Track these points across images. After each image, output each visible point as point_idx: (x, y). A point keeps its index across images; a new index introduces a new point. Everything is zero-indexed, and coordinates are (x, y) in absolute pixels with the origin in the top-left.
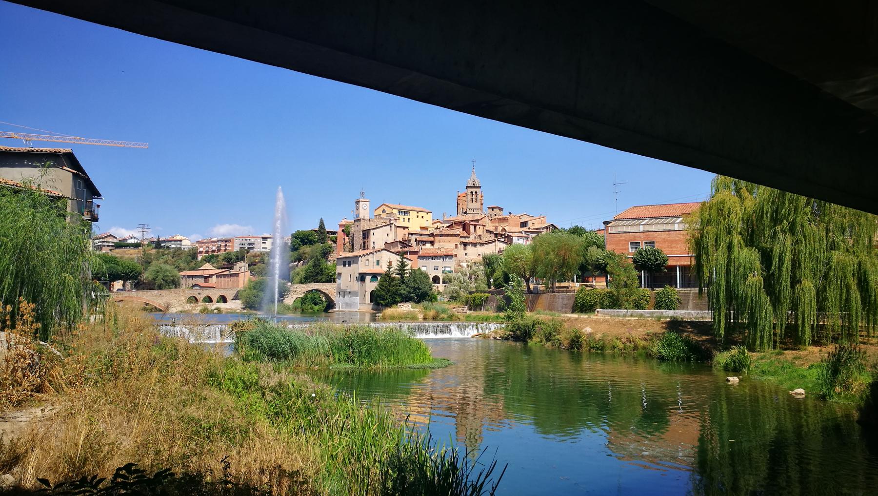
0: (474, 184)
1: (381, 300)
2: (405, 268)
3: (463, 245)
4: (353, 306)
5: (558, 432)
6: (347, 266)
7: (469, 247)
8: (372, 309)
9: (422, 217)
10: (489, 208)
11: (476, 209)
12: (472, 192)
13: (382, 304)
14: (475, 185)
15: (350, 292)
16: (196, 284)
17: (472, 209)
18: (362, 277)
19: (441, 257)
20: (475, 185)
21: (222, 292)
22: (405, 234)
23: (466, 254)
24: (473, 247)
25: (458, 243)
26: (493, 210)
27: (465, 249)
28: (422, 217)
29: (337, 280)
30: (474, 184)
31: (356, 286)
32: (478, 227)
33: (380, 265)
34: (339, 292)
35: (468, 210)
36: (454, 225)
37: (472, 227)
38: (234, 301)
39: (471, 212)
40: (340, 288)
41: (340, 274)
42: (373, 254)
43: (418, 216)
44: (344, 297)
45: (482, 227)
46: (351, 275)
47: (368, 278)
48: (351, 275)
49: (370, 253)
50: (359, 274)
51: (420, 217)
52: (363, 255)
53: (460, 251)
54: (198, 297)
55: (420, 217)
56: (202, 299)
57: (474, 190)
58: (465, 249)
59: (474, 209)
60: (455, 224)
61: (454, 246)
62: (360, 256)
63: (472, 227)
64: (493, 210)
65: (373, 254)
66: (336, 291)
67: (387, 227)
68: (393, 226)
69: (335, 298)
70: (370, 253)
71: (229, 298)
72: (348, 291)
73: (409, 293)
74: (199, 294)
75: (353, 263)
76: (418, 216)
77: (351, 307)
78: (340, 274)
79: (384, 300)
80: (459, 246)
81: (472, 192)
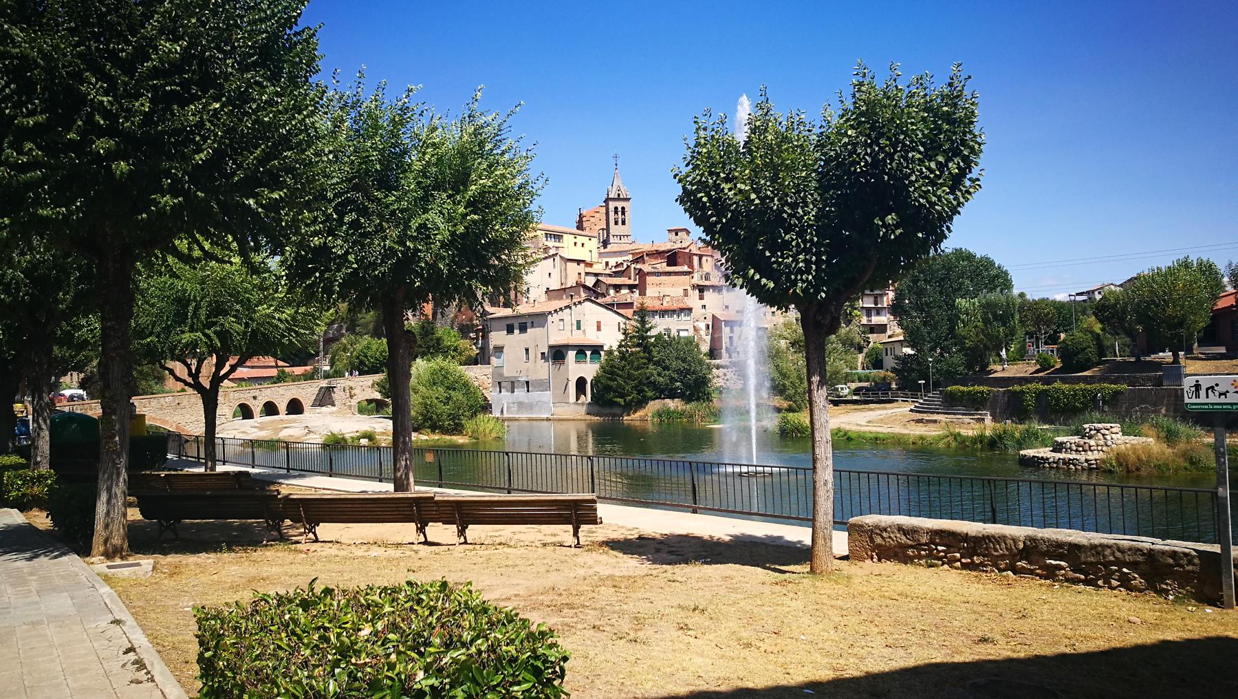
0: (619, 195)
1: (617, 397)
2: (649, 334)
3: (697, 291)
4: (536, 409)
5: (52, 552)
6: (517, 331)
7: (708, 294)
8: (588, 414)
9: (583, 245)
10: (670, 231)
11: (624, 236)
12: (616, 208)
13: (618, 404)
14: (621, 197)
15: (527, 383)
16: (177, 380)
17: (617, 236)
18: (557, 354)
19: (674, 311)
20: (621, 197)
21: (294, 392)
22: (580, 274)
23: (704, 307)
24: (716, 294)
25: (689, 288)
26: (677, 234)
27: (701, 298)
28: (583, 245)
29: (494, 360)
30: (619, 195)
31: (542, 370)
32: (704, 259)
33: (582, 328)
34: (499, 383)
35: (611, 237)
36: (646, 258)
37: (696, 259)
38: (319, 409)
39: (617, 240)
40: (501, 375)
41: (499, 350)
42: (570, 308)
43: (575, 243)
44: (513, 392)
45: (709, 259)
46: (527, 350)
47: (571, 354)
48: (527, 350)
49: (566, 307)
50: (551, 347)
51: (579, 244)
52: (556, 311)
53: (693, 300)
54: (251, 403)
55: (579, 244)
56: (259, 409)
57: (620, 205)
58: (701, 298)
59: (620, 236)
60: (647, 255)
61: (681, 293)
62: (550, 313)
63: (696, 259)
64: (677, 234)
65: (570, 308)
66: (490, 381)
67: (549, 260)
68: (557, 258)
69: (492, 395)
70: (566, 307)
71: (307, 403)
72: (524, 379)
73: (673, 380)
74: (255, 398)
75: (532, 327)
76: (575, 243)
77: (531, 410)
78: (499, 350)
79: (622, 396)
80: (690, 292)
81: (616, 208)
